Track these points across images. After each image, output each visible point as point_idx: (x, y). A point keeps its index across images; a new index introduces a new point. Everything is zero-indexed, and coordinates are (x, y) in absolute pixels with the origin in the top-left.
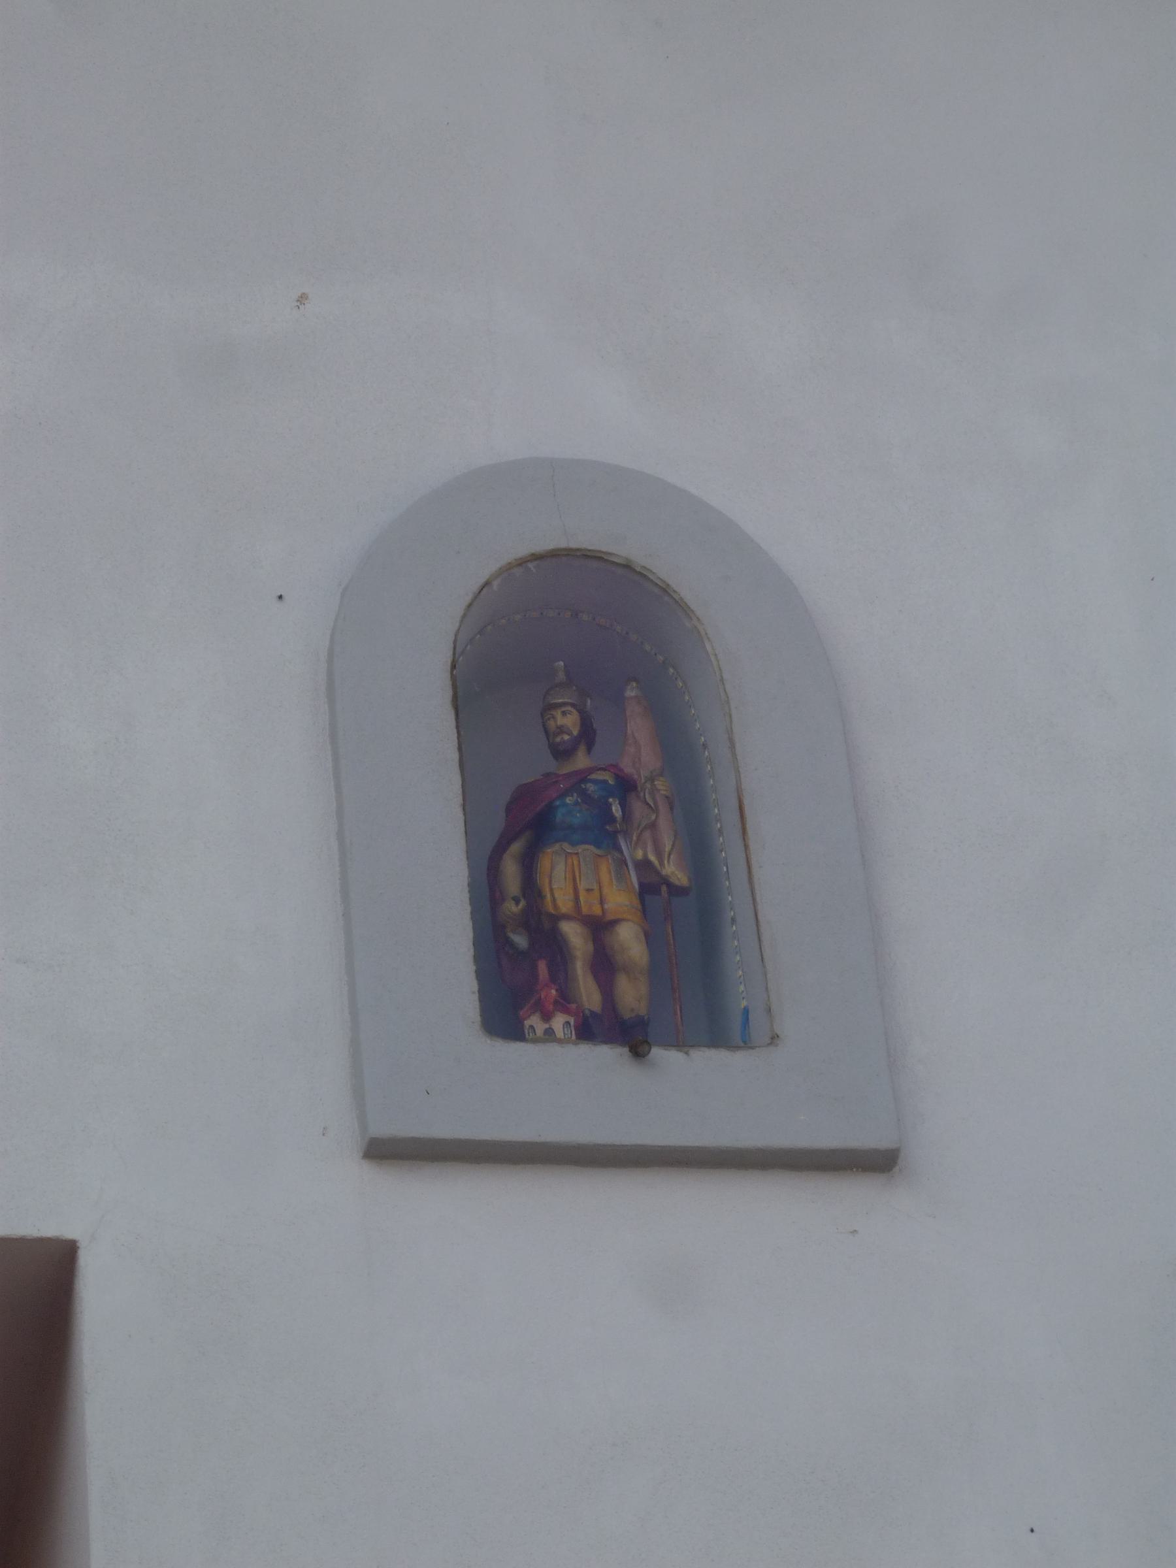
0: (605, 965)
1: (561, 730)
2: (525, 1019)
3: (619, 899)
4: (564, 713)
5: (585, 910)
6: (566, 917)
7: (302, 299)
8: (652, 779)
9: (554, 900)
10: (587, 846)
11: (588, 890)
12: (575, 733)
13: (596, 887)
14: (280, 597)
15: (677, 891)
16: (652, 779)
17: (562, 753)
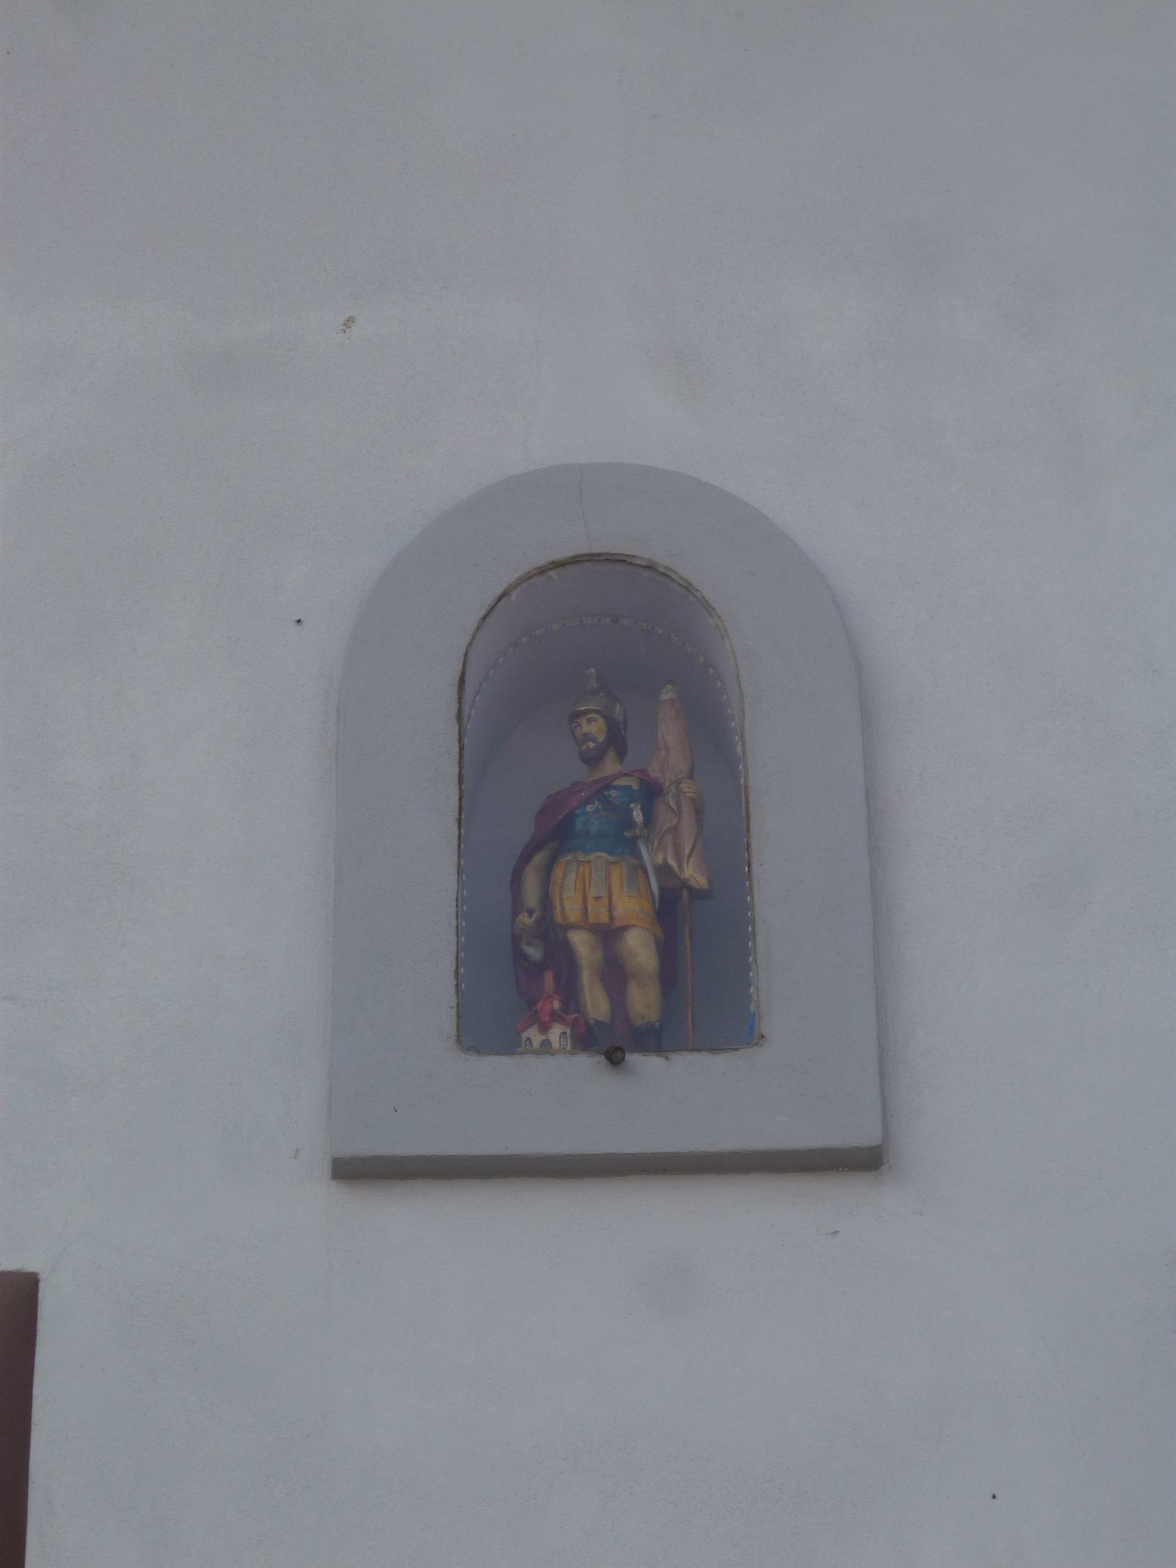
0: (615, 974)
1: (587, 738)
2: (523, 1031)
3: (629, 905)
4: (589, 721)
5: (591, 919)
6: (575, 927)
7: (349, 322)
8: (678, 782)
9: (563, 909)
10: (598, 854)
11: (598, 898)
12: (601, 739)
13: (604, 894)
14: (299, 621)
15: (697, 894)
16: (678, 782)
17: (592, 760)
